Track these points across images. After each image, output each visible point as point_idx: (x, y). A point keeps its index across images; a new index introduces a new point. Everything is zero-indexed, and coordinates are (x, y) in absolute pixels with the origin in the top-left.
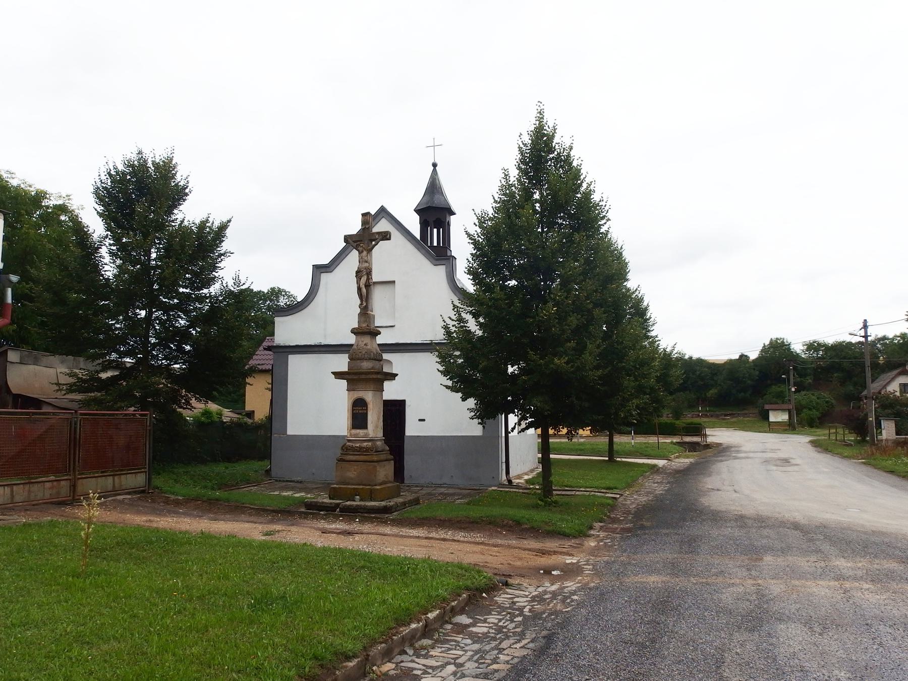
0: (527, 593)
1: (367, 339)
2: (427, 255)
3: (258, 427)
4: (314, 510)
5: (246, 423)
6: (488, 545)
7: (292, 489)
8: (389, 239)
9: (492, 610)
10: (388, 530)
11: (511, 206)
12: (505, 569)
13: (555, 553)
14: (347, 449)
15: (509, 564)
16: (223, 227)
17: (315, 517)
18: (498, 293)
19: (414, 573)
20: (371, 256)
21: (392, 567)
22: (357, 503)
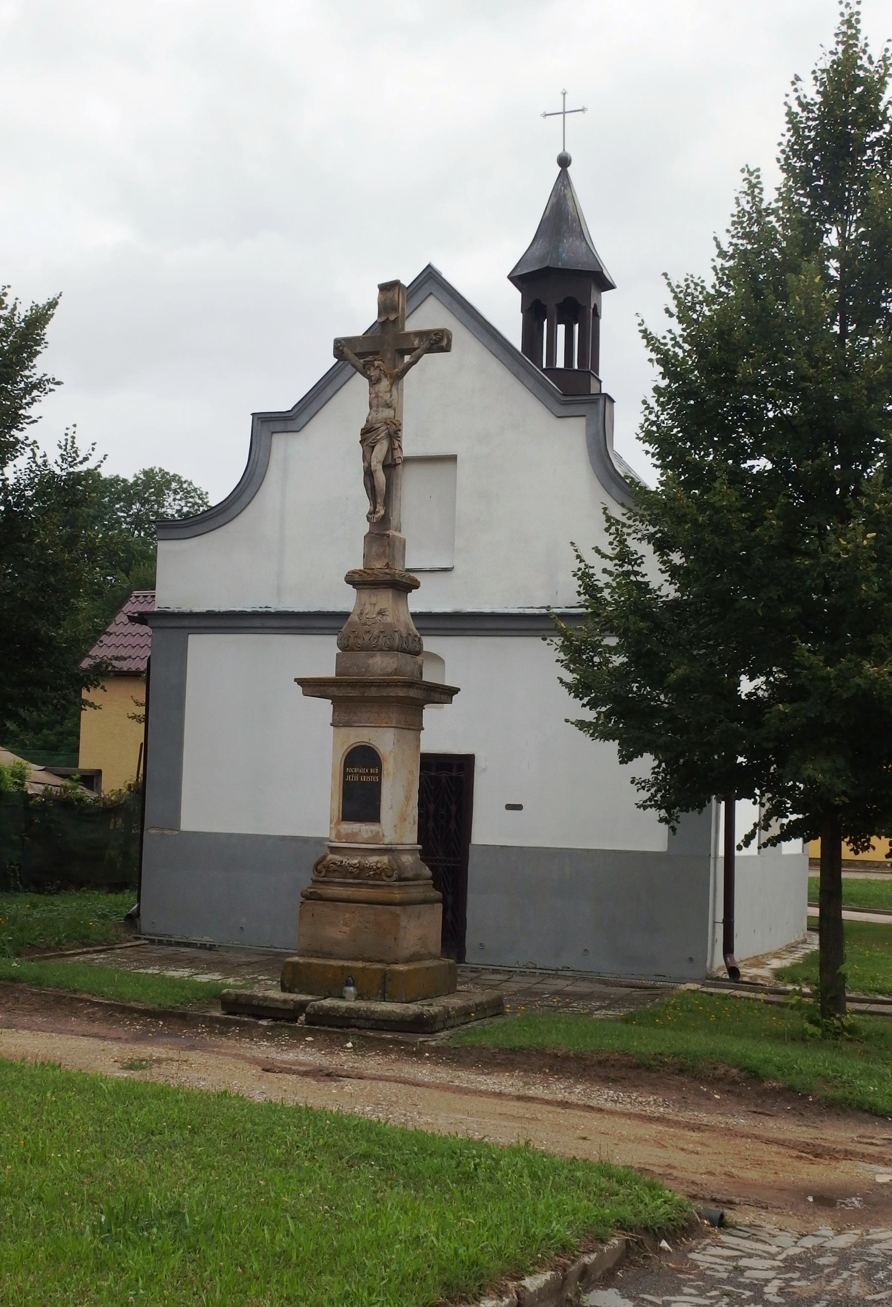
0: (773, 1249)
1: (384, 599)
2: (540, 391)
3: (111, 809)
4: (242, 1014)
5: (80, 800)
6: (677, 1124)
7: (191, 962)
8: (447, 349)
9: (684, 1283)
10: (423, 1072)
11: (764, 266)
12: (715, 1185)
13: (848, 1155)
14: (327, 868)
15: (729, 1175)
16: (40, 318)
17: (247, 1031)
18: (723, 494)
19: (490, 1180)
20: (400, 392)
21: (436, 1161)
22: (349, 1002)
